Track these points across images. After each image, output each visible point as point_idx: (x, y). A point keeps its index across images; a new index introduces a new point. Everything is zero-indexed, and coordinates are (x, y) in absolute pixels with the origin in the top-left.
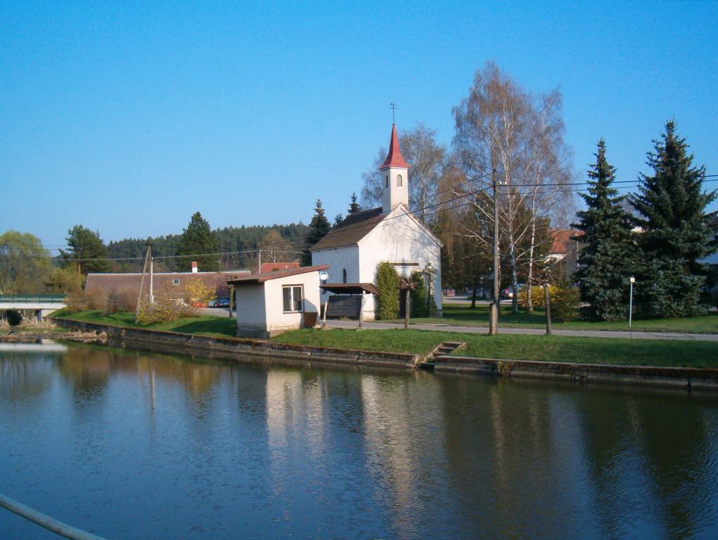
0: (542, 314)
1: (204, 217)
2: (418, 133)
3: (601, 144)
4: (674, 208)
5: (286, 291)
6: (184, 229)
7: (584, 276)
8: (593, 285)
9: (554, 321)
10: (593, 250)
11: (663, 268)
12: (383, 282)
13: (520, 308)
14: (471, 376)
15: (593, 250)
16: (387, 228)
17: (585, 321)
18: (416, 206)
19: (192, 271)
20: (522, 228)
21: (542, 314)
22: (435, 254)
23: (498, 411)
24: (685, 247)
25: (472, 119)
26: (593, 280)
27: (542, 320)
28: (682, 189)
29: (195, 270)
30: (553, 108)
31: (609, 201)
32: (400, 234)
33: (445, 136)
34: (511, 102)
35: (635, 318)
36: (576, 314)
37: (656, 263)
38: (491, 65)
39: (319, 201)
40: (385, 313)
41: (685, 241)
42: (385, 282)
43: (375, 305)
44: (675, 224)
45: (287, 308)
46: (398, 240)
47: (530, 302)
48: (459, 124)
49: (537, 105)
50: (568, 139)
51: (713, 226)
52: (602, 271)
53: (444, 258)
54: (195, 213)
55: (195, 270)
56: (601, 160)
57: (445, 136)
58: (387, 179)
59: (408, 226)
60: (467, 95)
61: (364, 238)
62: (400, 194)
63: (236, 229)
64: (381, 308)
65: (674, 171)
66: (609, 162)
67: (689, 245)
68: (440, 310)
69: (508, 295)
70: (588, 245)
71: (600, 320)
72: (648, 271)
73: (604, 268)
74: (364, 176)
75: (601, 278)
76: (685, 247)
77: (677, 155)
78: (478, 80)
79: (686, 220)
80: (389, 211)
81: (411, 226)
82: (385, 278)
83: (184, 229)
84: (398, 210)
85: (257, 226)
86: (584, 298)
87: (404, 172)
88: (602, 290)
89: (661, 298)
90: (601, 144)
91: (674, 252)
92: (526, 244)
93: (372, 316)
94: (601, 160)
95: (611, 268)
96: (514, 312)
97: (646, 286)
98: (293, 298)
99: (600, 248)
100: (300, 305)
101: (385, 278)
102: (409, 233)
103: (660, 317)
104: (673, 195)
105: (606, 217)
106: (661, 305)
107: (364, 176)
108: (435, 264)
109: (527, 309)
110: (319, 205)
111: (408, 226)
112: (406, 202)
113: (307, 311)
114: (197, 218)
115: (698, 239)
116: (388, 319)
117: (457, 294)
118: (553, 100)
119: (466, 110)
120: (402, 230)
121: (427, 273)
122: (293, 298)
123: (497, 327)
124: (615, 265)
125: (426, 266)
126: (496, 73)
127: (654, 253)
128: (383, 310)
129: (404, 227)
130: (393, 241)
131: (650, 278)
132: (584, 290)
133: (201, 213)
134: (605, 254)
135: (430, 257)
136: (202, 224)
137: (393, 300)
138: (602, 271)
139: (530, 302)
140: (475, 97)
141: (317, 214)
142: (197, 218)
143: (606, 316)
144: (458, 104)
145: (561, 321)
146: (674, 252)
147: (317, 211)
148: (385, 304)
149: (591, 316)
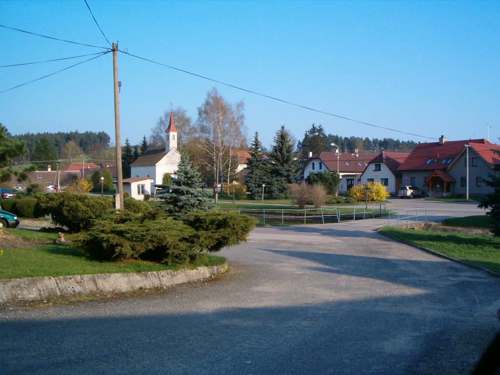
0: (232, 196)
2: (179, 111)
3: (257, 133)
4: (282, 159)
5: (139, 187)
7: (248, 183)
8: (251, 186)
9: (235, 199)
10: (252, 173)
11: (277, 181)
13: (224, 194)
15: (252, 173)
17: (249, 199)
20: (225, 161)
21: (232, 196)
23: (216, 267)
24: (286, 173)
25: (206, 112)
26: (252, 184)
27: (231, 199)
28: (285, 153)
29: (49, 170)
30: (241, 109)
31: (258, 155)
33: (193, 116)
34: (222, 108)
35: (265, 198)
36: (245, 197)
37: (274, 179)
38: (214, 107)
41: (285, 171)
44: (282, 165)
45: (139, 193)
47: (228, 191)
48: (200, 114)
49: (234, 108)
50: (246, 122)
51: (1, 282)
52: (255, 181)
55: (49, 170)
56: (256, 139)
57: (193, 116)
58: (168, 137)
60: (204, 102)
61: (159, 162)
62: (173, 143)
63: (33, 135)
65: (283, 145)
66: (259, 140)
67: (287, 173)
70: (250, 171)
71: (254, 199)
72: (271, 182)
73: (256, 180)
74: (152, 130)
75: (255, 184)
76: (286, 173)
77: (284, 139)
78: (209, 95)
79: (286, 163)
80: (169, 151)
84: (173, 150)
85: (46, 133)
86: (248, 191)
87: (175, 134)
88: (255, 188)
89: (276, 192)
90: (257, 133)
91: (281, 175)
92: (227, 167)
94: (256, 139)
95: (258, 180)
96: (221, 196)
97: (270, 187)
98: (141, 190)
99: (254, 172)
100: (143, 192)
103: (276, 198)
104: (282, 154)
105: (257, 161)
106: (276, 194)
107: (152, 130)
109: (226, 194)
110: (127, 141)
112: (176, 147)
113: (146, 194)
115: (290, 171)
118: (240, 105)
119: (203, 109)
122: (141, 190)
123: (218, 201)
124: (260, 179)
126: (216, 93)
127: (274, 175)
131: (272, 184)
132: (248, 188)
134: (256, 175)
138: (255, 181)
139: (228, 191)
140: (207, 103)
141: (126, 145)
143: (256, 198)
144: (200, 106)
145: (239, 199)
146: (281, 175)
147: (126, 144)
149: (251, 197)
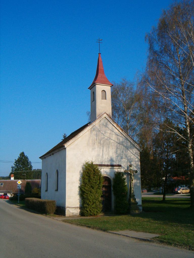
1: (26, 154)
6: (15, 160)
12: (87, 181)
14: (124, 137)
16: (94, 133)
18: (118, 112)
19: (11, 179)
22: (136, 155)
32: (106, 138)
39: (65, 134)
40: (88, 209)
42: (89, 181)
43: (80, 202)
46: (103, 143)
53: (144, 156)
54: (22, 152)
59: (113, 131)
64: (85, 205)
68: (140, 206)
69: (177, 191)
81: (114, 133)
82: (89, 177)
83: (15, 160)
87: (108, 89)
93: (77, 212)
101: (89, 177)
102: (114, 137)
108: (136, 164)
111: (113, 131)
114: (22, 154)
116: (91, 215)
117: (148, 191)
120: (107, 135)
121: (129, 173)
125: (128, 168)
128: (86, 207)
129: (109, 132)
130: (100, 143)
133: (24, 152)
135: (131, 160)
136: (25, 158)
137: (97, 196)
142: (22, 154)
148: (88, 202)
